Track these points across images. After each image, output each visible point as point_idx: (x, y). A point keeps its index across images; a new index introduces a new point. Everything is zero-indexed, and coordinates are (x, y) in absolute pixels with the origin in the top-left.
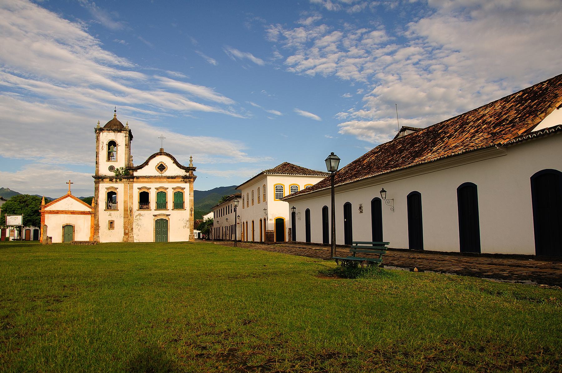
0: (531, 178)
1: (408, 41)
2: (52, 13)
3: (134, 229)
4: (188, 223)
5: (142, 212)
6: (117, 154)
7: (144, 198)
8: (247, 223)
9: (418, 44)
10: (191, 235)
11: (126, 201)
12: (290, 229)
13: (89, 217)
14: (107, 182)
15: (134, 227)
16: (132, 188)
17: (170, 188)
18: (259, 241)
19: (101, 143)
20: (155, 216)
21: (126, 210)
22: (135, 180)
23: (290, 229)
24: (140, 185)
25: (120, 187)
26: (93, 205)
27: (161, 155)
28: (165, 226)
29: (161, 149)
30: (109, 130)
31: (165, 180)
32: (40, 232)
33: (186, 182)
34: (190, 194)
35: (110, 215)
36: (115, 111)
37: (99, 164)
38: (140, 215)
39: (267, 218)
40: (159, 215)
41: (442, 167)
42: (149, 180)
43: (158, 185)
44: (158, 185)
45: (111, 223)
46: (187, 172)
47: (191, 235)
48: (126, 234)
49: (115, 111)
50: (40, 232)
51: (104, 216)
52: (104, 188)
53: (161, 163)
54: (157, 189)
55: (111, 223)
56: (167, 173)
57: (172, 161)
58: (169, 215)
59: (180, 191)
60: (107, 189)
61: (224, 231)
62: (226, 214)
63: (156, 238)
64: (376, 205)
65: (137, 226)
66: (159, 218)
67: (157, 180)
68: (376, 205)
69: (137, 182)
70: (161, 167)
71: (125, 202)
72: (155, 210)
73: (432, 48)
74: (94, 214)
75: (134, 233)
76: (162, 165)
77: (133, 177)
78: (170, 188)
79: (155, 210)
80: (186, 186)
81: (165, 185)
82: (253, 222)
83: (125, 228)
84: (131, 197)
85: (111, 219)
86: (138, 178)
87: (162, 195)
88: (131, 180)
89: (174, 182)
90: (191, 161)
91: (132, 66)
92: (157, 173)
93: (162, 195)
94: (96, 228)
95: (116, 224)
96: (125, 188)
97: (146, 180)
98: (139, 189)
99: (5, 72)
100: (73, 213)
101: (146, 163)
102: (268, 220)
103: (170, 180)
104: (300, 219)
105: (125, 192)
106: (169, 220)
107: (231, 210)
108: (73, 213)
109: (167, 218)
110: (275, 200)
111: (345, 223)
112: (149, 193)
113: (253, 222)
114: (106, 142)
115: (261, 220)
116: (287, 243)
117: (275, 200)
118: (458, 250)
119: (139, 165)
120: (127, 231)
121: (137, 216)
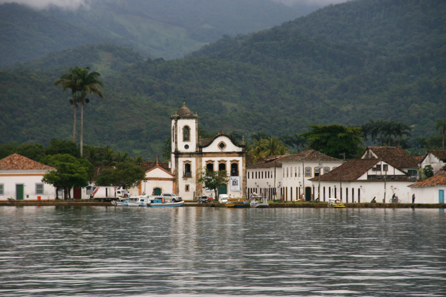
2: (156, 54)
8: (287, 188)
16: (201, 161)
17: (228, 161)
22: (203, 155)
25: (193, 161)
31: (224, 155)
33: (240, 156)
34: (243, 165)
35: (185, 182)
41: (192, 274)
42: (213, 155)
43: (220, 159)
45: (187, 188)
51: (182, 183)
52: (181, 160)
53: (221, 142)
54: (219, 161)
55: (187, 188)
56: (227, 150)
59: (211, 163)
62: (266, 177)
63: (368, 178)
69: (205, 157)
70: (222, 145)
74: (175, 180)
78: (228, 161)
81: (225, 158)
82: (291, 188)
85: (186, 184)
86: (205, 153)
87: (222, 166)
88: (200, 155)
91: (398, 173)
92: (218, 150)
93: (222, 166)
94: (176, 191)
95: (190, 188)
96: (196, 161)
97: (211, 155)
98: (207, 162)
99: (422, 181)
100: (160, 179)
103: (228, 155)
105: (197, 164)
108: (160, 179)
112: (433, 176)
113: (291, 188)
115: (297, 188)
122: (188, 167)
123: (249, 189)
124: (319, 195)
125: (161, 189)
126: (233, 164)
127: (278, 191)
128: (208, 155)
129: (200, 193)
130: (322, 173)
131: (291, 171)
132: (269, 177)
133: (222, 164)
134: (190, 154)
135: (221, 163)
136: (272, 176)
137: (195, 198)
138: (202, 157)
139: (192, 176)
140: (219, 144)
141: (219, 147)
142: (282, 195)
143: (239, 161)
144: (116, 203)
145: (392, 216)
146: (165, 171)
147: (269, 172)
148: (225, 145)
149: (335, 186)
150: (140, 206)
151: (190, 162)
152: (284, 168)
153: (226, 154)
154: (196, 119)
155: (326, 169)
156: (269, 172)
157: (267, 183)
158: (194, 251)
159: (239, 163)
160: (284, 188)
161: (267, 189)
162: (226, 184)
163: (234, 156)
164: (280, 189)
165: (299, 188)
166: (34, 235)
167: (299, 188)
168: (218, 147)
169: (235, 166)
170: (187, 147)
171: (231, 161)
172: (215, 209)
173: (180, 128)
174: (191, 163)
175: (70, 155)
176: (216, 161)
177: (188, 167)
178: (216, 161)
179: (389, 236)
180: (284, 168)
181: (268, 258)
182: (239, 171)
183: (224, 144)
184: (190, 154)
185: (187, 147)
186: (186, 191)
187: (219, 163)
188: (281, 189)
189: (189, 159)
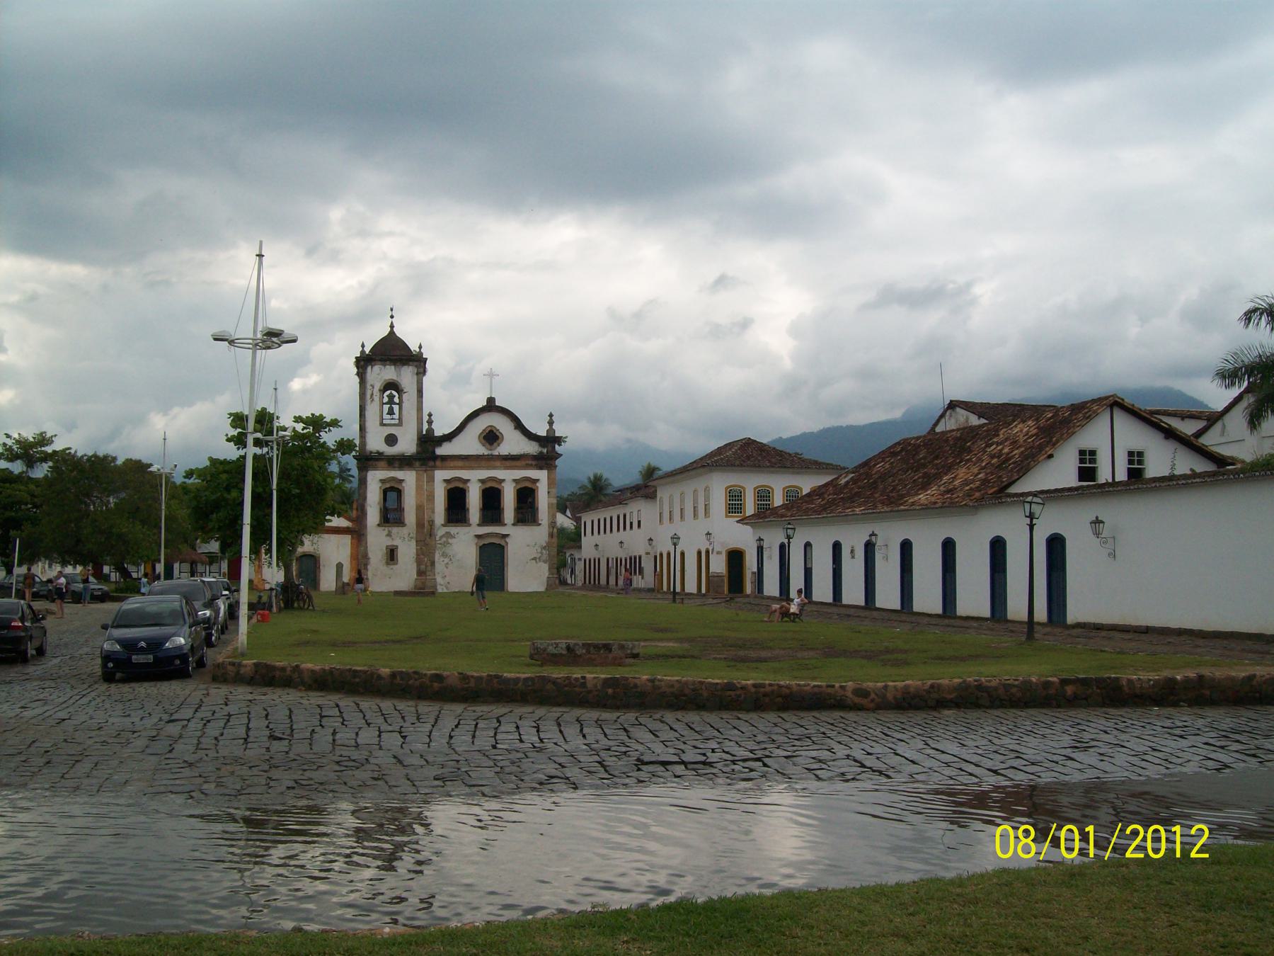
0: (991, 542)
3: (436, 565)
4: (544, 551)
5: (453, 530)
7: (456, 498)
11: (420, 506)
12: (753, 573)
13: (347, 539)
14: (383, 469)
15: (436, 559)
16: (431, 480)
17: (509, 479)
18: (695, 591)
19: (369, 387)
20: (478, 537)
21: (420, 525)
22: (438, 463)
23: (753, 573)
24: (449, 474)
25: (409, 478)
27: (489, 411)
29: (491, 400)
30: (385, 361)
31: (498, 463)
33: (541, 468)
36: (392, 317)
37: (367, 430)
38: (448, 535)
39: (713, 549)
40: (488, 535)
42: (467, 463)
45: (392, 555)
46: (541, 446)
48: (420, 573)
49: (392, 317)
51: (377, 539)
52: (375, 479)
53: (489, 429)
54: (482, 481)
55: (392, 555)
56: (504, 449)
58: (508, 535)
59: (461, 486)
60: (382, 481)
61: (610, 565)
62: (618, 530)
63: (1129, 479)
64: (869, 548)
65: (442, 559)
66: (487, 541)
67: (483, 463)
68: (869, 548)
69: (442, 468)
70: (491, 437)
71: (420, 508)
72: (479, 525)
75: (437, 571)
76: (491, 431)
77: (435, 458)
78: (509, 479)
79: (479, 525)
80: (542, 475)
81: (499, 474)
83: (419, 561)
84: (431, 498)
85: (390, 543)
86: (444, 458)
87: (492, 497)
88: (431, 463)
90: (551, 423)
93: (492, 497)
96: (418, 480)
97: (460, 463)
102: (715, 553)
103: (508, 463)
104: (770, 557)
105: (419, 488)
107: (631, 523)
109: (503, 543)
110: (727, 516)
111: (834, 570)
114: (378, 386)
115: (699, 553)
116: (748, 596)
117: (727, 516)
118: (899, 608)
119: (446, 433)
120: (423, 567)
121: (441, 537)
122: (392, 491)
123: (585, 560)
124: (808, 573)
125: (319, 557)
126: (521, 489)
127: (648, 565)
128: (452, 464)
129: (429, 568)
130: (778, 500)
131: (682, 501)
132: (625, 528)
134: (402, 462)
135: (489, 485)
136: (631, 523)
137: (340, 584)
138: (435, 467)
139: (407, 521)
141: (484, 441)
142: (658, 576)
143: (538, 480)
144: (30, 607)
145: (34, 438)
147: (625, 516)
149: (760, 540)
151: (401, 481)
152: (661, 498)
153: (504, 462)
154: (415, 363)
155: (791, 493)
156: (625, 516)
157: (621, 543)
159: (537, 487)
160: (661, 555)
161: (621, 560)
163: (527, 467)
164: (653, 559)
165: (707, 552)
167: (707, 552)
168: (481, 442)
169: (526, 496)
170: (391, 440)
171: (515, 480)
173: (373, 387)
174: (404, 484)
176: (475, 481)
177: (392, 491)
178: (475, 481)
180: (661, 498)
182: (538, 509)
183: (498, 434)
184: (402, 462)
185: (391, 440)
186: (388, 564)
187: (484, 487)
188: (656, 557)
189: (399, 474)
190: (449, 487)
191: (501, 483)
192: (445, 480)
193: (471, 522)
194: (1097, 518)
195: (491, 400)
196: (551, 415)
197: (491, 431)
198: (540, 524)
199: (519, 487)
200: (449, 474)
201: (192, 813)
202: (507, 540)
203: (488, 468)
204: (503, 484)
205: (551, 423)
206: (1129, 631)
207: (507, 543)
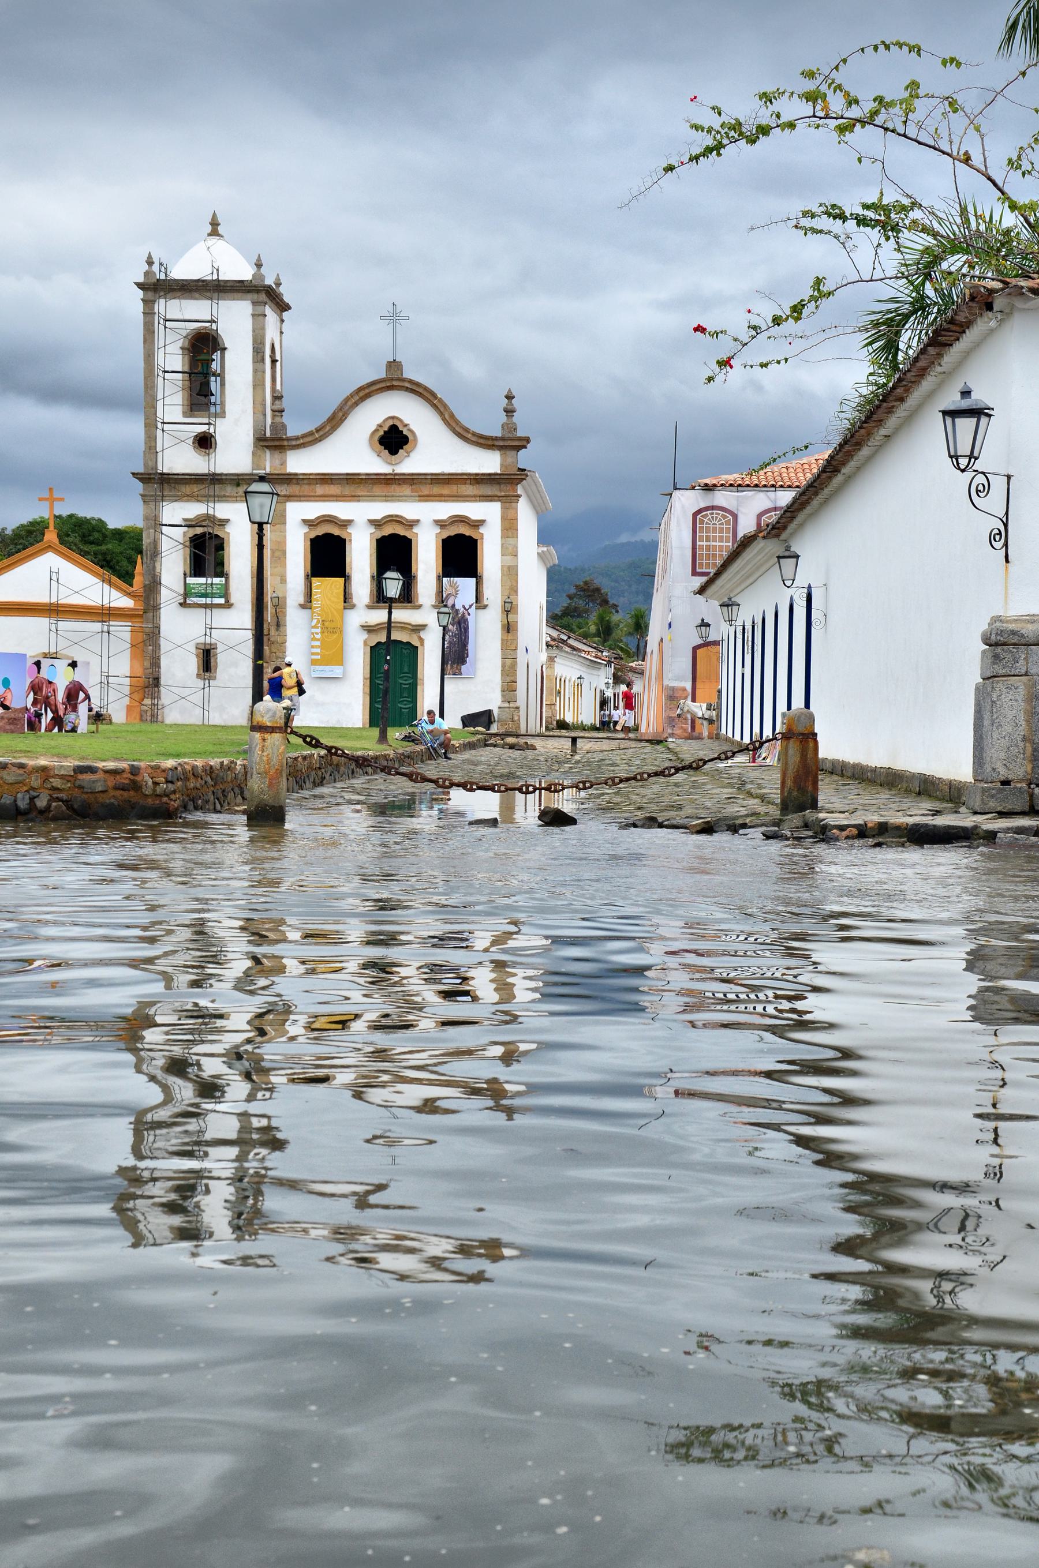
1: (584, 590)
6: (223, 384)
9: (323, 797)
10: (507, 705)
11: (509, 567)
13: (122, 632)
24: (314, 510)
26: (138, 581)
28: (406, 669)
29: (394, 365)
32: (792, 1103)
43: (380, 510)
44: (380, 510)
45: (207, 659)
47: (507, 705)
50: (792, 1103)
54: (375, 523)
55: (207, 659)
56: (412, 463)
57: (149, 1160)
72: (369, 607)
73: (873, 419)
76: (394, 429)
79: (369, 607)
81: (408, 510)
89: (441, 496)
90: (509, 412)
92: (374, 463)
101: (335, 421)
106: (422, 644)
128: (187, 489)
133: (394, 537)
135: (388, 531)
140: (376, 431)
143: (228, 521)
146: (252, 598)
148: (411, 437)
150: (687, 817)
158: (425, 980)
162: (415, 642)
166: (98, 1341)
171: (372, 522)
172: (795, 762)
175: (633, 540)
179: (643, 744)
181: (475, 915)
183: (405, 432)
185: (205, 442)
190: (313, 535)
191: (411, 526)
192: (305, 521)
193: (421, 601)
194: (703, 620)
195: (394, 365)
196: (510, 397)
197: (394, 429)
198: (420, 606)
199: (313, 535)
200: (314, 510)
201: (1016, 1040)
202: (422, 634)
203: (387, 498)
204: (415, 530)
205: (509, 412)
206: (862, 832)
207: (422, 640)
